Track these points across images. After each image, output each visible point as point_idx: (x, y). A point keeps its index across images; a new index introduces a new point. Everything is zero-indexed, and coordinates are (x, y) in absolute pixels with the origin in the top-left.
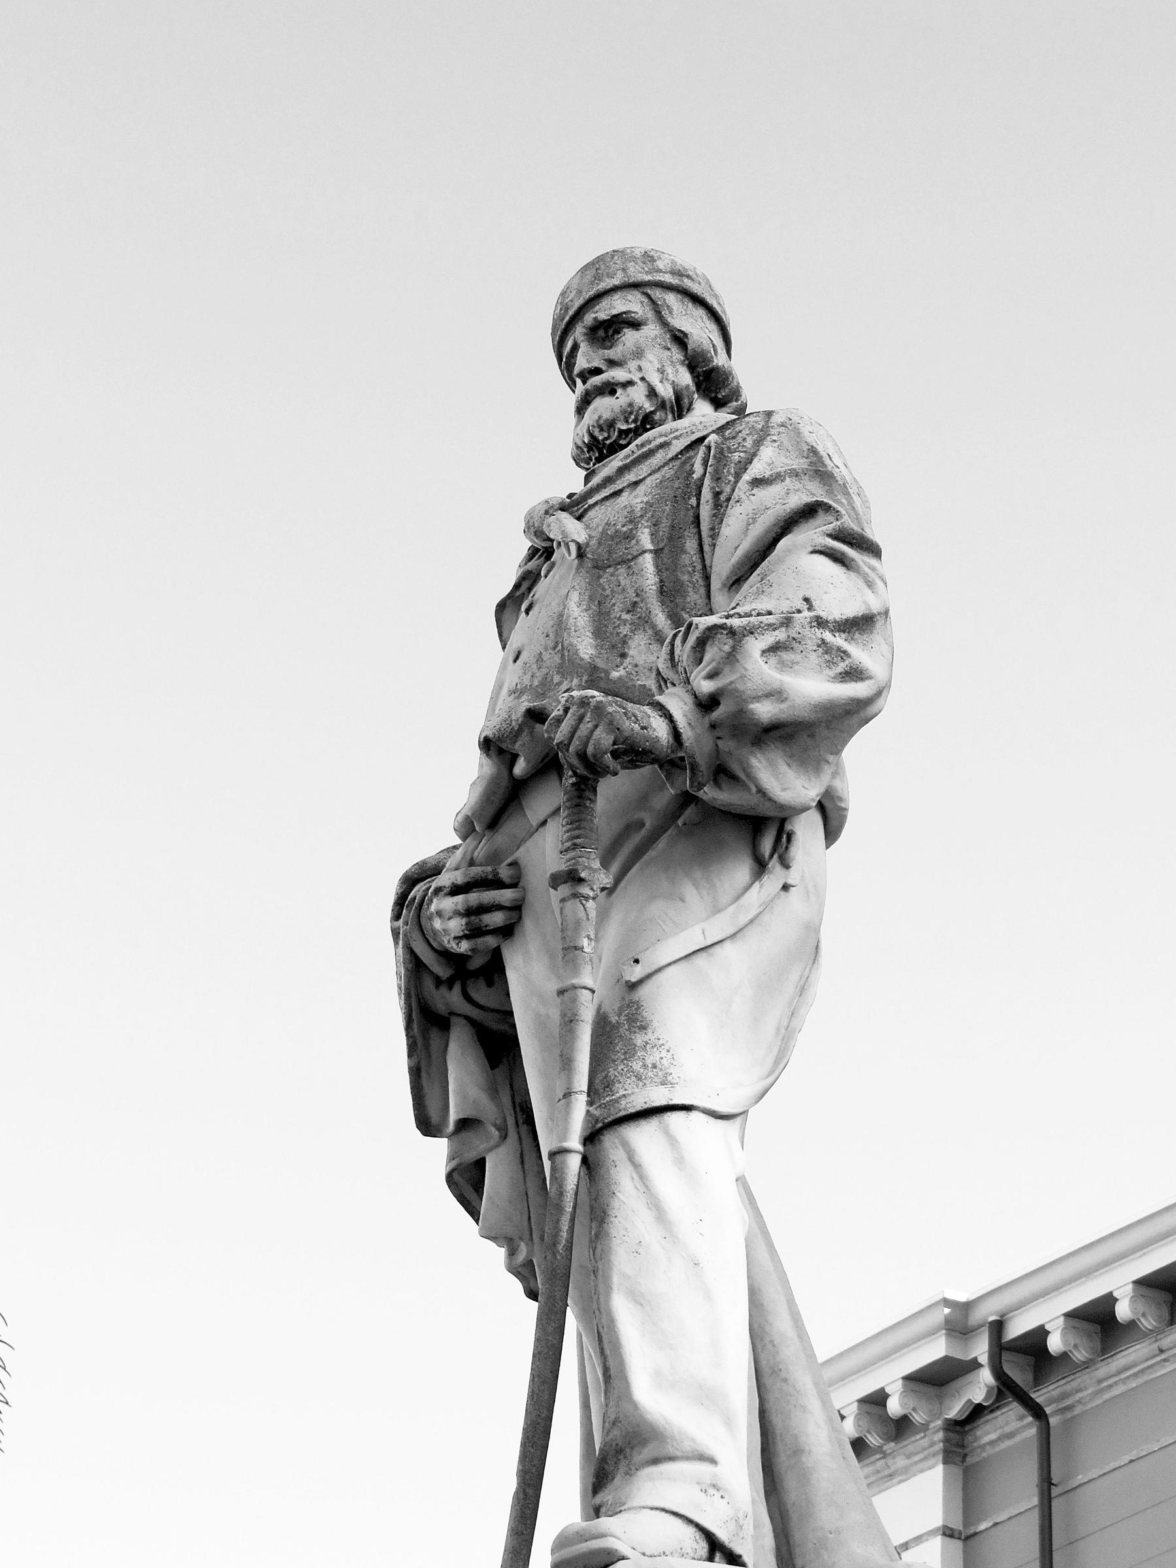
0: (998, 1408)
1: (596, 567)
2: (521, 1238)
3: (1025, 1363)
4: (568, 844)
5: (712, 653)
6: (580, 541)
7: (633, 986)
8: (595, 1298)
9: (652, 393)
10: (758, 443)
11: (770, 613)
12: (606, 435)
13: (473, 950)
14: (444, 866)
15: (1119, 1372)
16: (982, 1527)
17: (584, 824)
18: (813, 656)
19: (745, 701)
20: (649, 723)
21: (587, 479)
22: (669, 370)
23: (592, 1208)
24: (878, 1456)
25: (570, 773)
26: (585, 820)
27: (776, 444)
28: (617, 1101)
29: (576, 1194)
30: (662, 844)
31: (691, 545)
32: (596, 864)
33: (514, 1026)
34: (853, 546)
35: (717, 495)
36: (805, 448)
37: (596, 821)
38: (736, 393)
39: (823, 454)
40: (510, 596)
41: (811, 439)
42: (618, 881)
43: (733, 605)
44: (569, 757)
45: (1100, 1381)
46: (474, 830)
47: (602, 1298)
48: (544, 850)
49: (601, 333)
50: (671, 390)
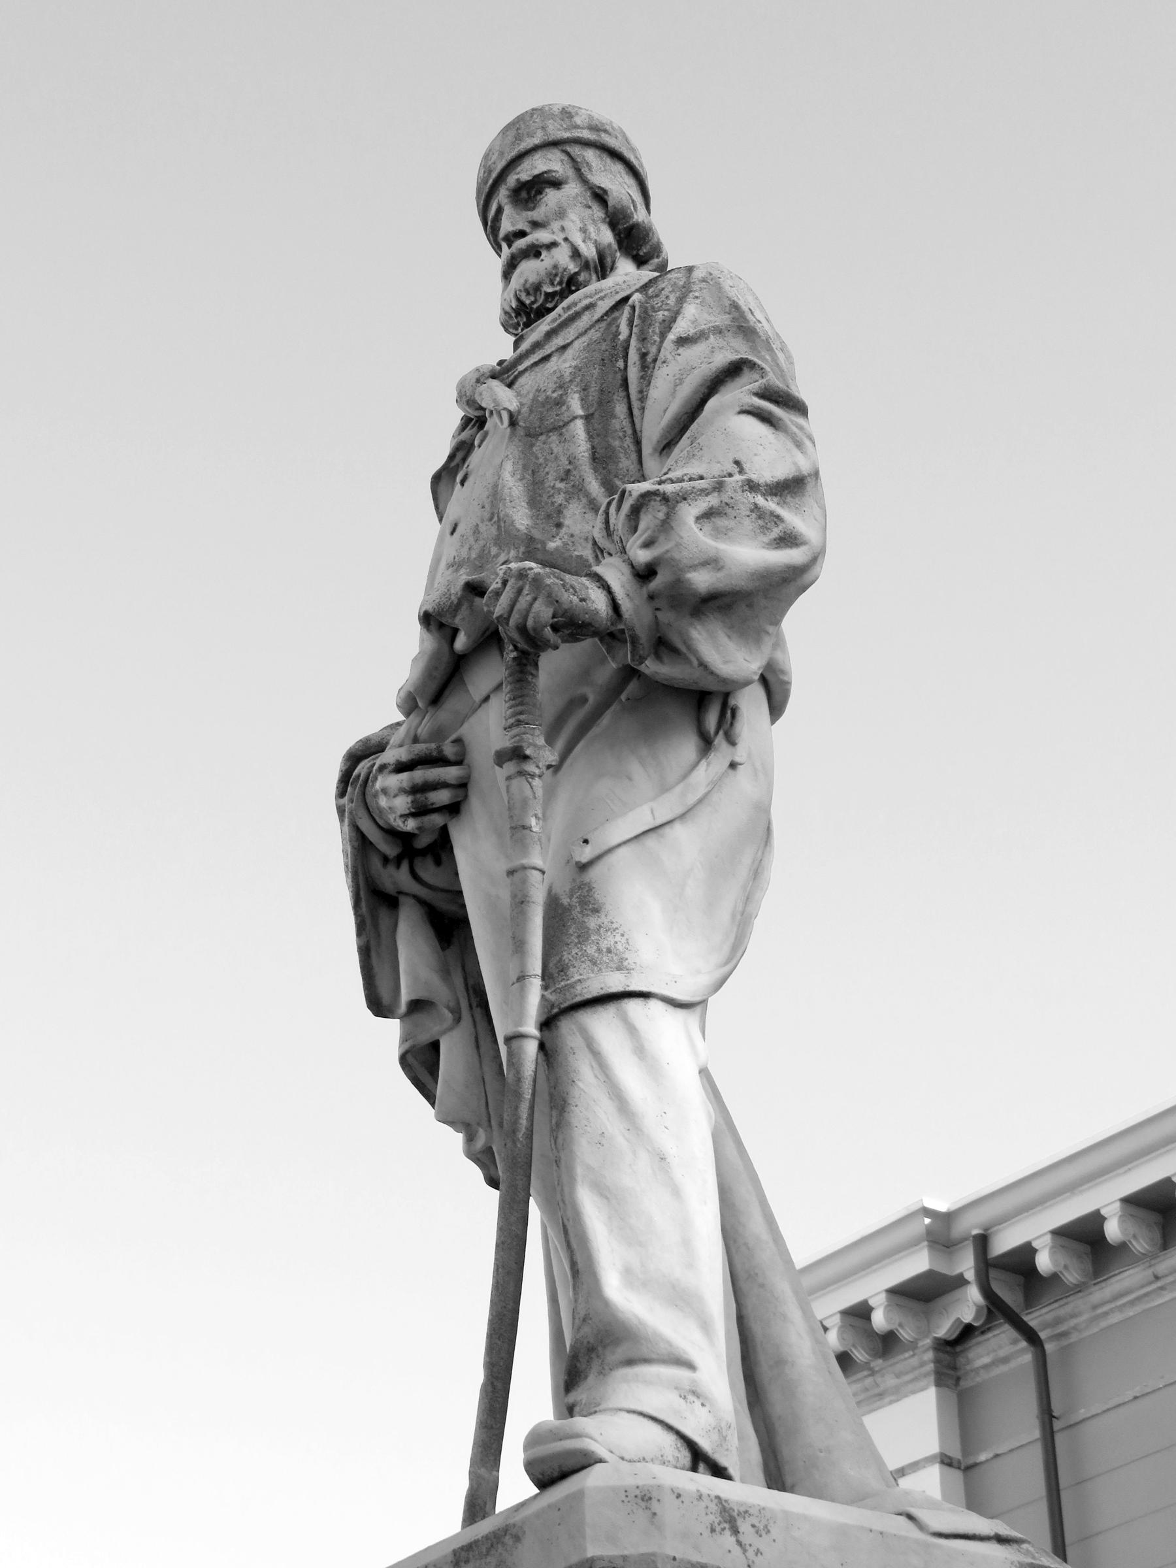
0: (989, 1329)
1: (528, 435)
2: (479, 1124)
3: (1014, 1282)
4: (512, 721)
5: (647, 521)
6: (512, 408)
7: (583, 867)
8: (559, 1189)
9: (576, 254)
10: (681, 300)
11: (701, 478)
12: (532, 299)
13: (419, 828)
14: (387, 743)
15: (1116, 1298)
16: (983, 1457)
17: (527, 699)
18: (747, 522)
19: (681, 570)
20: (587, 594)
21: (516, 345)
22: (591, 229)
23: (551, 1096)
24: (866, 1373)
25: (511, 647)
26: (527, 695)
27: (698, 301)
28: (572, 986)
29: (535, 1081)
30: (606, 720)
31: (620, 409)
32: (541, 741)
33: (464, 906)
34: (779, 404)
35: (643, 356)
36: (727, 303)
37: (539, 696)
38: (657, 250)
39: (745, 308)
40: (445, 468)
41: (732, 293)
42: (564, 757)
43: (665, 470)
44: (509, 632)
45: (1095, 1307)
46: (416, 706)
47: (566, 1189)
48: (487, 727)
49: (524, 194)
50: (594, 250)
